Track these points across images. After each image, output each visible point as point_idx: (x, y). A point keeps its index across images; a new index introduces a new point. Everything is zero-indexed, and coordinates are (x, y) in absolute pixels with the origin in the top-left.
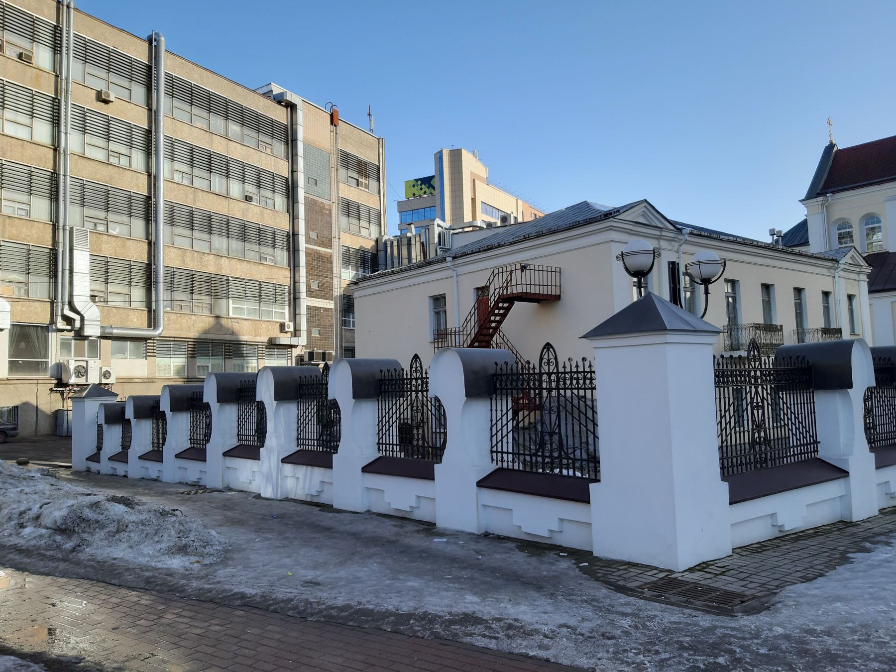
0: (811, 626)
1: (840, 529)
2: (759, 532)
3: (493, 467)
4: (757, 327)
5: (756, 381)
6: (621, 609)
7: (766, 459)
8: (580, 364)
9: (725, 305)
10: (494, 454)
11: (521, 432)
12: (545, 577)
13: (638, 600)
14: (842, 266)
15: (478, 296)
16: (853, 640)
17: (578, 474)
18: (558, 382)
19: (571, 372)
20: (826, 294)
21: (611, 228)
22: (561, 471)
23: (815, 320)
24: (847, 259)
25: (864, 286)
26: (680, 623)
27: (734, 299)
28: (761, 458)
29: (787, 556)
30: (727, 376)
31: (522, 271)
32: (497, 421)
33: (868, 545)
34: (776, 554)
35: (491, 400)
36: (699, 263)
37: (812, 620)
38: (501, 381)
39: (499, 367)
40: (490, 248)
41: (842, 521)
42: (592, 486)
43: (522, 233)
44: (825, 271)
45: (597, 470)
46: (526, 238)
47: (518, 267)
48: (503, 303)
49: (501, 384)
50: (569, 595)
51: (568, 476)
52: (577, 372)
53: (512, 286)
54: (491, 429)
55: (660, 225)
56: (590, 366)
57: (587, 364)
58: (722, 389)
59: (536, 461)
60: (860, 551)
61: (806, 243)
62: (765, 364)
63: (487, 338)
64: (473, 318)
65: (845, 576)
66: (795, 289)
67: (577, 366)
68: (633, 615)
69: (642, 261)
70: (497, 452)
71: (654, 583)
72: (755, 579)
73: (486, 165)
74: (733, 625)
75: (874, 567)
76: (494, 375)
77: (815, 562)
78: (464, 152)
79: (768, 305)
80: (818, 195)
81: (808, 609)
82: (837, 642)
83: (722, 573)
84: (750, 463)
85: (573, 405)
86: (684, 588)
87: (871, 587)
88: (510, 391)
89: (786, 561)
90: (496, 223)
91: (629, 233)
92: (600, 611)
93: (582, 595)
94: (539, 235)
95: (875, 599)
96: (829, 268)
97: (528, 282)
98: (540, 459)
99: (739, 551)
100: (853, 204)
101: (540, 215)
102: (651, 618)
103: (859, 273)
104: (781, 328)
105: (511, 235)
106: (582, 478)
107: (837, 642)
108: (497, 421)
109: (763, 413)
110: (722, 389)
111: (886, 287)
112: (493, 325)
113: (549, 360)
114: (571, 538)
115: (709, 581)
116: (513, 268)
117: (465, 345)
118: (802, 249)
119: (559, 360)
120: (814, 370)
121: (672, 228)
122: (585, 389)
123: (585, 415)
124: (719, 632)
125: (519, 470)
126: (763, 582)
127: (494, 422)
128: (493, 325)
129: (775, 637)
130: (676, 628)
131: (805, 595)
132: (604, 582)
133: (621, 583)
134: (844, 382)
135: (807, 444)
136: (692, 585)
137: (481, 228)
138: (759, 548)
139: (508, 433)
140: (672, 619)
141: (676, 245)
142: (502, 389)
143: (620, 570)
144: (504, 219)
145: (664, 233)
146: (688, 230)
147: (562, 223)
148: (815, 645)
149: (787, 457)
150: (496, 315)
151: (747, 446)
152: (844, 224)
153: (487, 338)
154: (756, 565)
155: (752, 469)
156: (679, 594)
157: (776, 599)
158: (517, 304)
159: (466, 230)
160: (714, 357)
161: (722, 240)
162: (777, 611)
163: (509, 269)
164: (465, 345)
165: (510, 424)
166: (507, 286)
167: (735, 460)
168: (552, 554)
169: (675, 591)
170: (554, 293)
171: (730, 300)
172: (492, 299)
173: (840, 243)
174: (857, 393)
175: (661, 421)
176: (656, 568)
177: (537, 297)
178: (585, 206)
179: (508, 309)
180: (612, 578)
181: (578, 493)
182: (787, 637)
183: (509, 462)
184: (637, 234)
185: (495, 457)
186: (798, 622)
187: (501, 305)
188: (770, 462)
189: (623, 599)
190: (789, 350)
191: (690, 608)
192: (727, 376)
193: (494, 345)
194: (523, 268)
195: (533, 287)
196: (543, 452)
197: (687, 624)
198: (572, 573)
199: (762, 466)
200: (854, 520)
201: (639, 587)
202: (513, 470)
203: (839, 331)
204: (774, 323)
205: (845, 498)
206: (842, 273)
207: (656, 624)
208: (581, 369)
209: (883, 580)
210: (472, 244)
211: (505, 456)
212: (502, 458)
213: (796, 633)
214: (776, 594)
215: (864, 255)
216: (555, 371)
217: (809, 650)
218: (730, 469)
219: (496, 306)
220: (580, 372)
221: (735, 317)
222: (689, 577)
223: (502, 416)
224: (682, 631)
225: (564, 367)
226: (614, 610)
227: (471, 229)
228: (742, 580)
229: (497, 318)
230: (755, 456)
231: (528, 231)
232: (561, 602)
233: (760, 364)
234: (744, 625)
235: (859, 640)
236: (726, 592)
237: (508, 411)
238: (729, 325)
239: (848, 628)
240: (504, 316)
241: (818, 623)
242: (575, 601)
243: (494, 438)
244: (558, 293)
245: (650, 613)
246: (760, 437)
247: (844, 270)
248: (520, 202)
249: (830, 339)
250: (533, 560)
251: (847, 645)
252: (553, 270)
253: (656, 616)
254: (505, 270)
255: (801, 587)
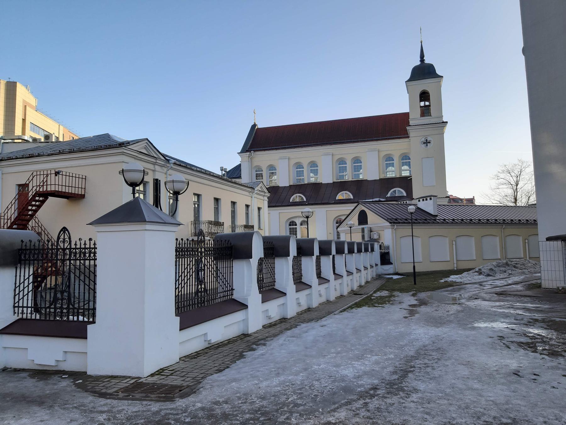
0: (218, 399)
1: (241, 339)
2: (196, 346)
3: (16, 318)
4: (210, 223)
5: (201, 254)
6: (100, 409)
7: (204, 301)
8: (88, 242)
9: (193, 209)
10: (16, 309)
11: (48, 291)
12: (48, 394)
13: (113, 401)
14: (256, 192)
15: (19, 190)
16: (239, 403)
17: (81, 318)
18: (70, 255)
19: (80, 248)
20: (247, 206)
21: (123, 154)
22: (68, 318)
23: (241, 220)
24: (258, 188)
25: (266, 203)
26: (139, 411)
27: (198, 205)
28: (201, 300)
29: (211, 358)
30: (184, 251)
31: (56, 175)
32: (20, 284)
33: (254, 346)
34: (205, 358)
35: (16, 268)
36: (173, 181)
37: (219, 396)
38: (25, 254)
39: (24, 244)
40: (31, 156)
41: (243, 334)
42: (89, 327)
43: (57, 149)
44: (247, 193)
45: (94, 315)
46: (60, 153)
47: (53, 172)
48: (40, 197)
49: (25, 257)
50: (64, 406)
51: (73, 321)
52: (85, 248)
53: (47, 185)
54: (15, 290)
55: (155, 156)
56: (95, 244)
57: (92, 242)
58: (186, 259)
59: (50, 312)
60: (250, 350)
61: (240, 177)
62: (207, 244)
63: (24, 223)
64: (13, 207)
65: (240, 366)
66: (232, 202)
67: (85, 244)
68: (108, 411)
69: (137, 177)
70: (18, 307)
71: (127, 387)
72: (191, 375)
73: (36, 97)
74: (172, 407)
75: (255, 359)
76: (19, 250)
77: (226, 360)
78: (19, 85)
79: (217, 210)
80: (247, 151)
81: (218, 389)
82: (230, 406)
83: (171, 374)
84: (195, 304)
85: (90, 271)
86: (145, 388)
87: (252, 371)
88: (32, 262)
89: (210, 361)
90: (40, 139)
91: (135, 158)
92: (85, 413)
93: (74, 404)
94: (71, 152)
95: (252, 377)
96: (250, 192)
97: (64, 184)
98: (52, 310)
99: (184, 358)
100: (265, 158)
101: (76, 138)
102: (120, 412)
103: (264, 196)
104: (223, 224)
105: (50, 148)
106: (83, 321)
107: (230, 406)
108: (20, 284)
109: (204, 273)
110: (186, 259)
111: (277, 205)
112: (30, 213)
113: (64, 239)
114: (72, 365)
115: (161, 381)
116: (49, 172)
117: (5, 227)
118: (237, 180)
119: (72, 239)
120: (232, 249)
121: (163, 159)
122: (90, 260)
123: (90, 276)
124: (163, 413)
125: (35, 319)
126: (194, 376)
127: (18, 285)
128: (30, 213)
129: (196, 410)
130: (136, 416)
131: (217, 381)
132: (92, 392)
133: (104, 391)
134: (249, 256)
135: (228, 291)
136: (151, 385)
137: (27, 141)
138: (196, 355)
139: (28, 292)
140: (134, 410)
141: (165, 169)
142: (25, 260)
143: (104, 382)
144: (47, 137)
145: (158, 161)
146: (173, 161)
147: (89, 146)
148: (218, 411)
149: (216, 299)
150: (33, 206)
151: (194, 295)
152: (259, 169)
153: (24, 223)
154: (193, 366)
155: (193, 308)
156: (141, 392)
157: (201, 385)
158: (50, 199)
159: (16, 141)
160: (177, 239)
161: (193, 170)
162: (200, 393)
163: (45, 173)
164: (5, 227)
165: (31, 286)
166: (43, 186)
167: (186, 302)
168: (56, 377)
169: (139, 391)
170: (80, 193)
171: (196, 206)
172: (30, 194)
173: (257, 179)
174: (290, 258)
175: (135, 280)
176: (129, 377)
177: (66, 195)
178: (107, 136)
179: (43, 202)
180: (97, 389)
181: (80, 332)
182: (203, 409)
183: (28, 314)
184: (141, 160)
185: (16, 311)
186: (210, 398)
187: (37, 198)
188: (206, 303)
189: (103, 401)
190: (228, 236)
191: (147, 400)
192: (184, 251)
193: (30, 228)
194: (57, 173)
195: (64, 187)
196: (55, 306)
197: (144, 411)
198: (69, 389)
199: (201, 305)
200: (250, 333)
201: (116, 392)
202: (31, 319)
203: (252, 227)
204: (220, 221)
205: (245, 321)
206: (256, 195)
207: (123, 415)
208: (87, 246)
209: (259, 365)
210: (17, 152)
211: (25, 309)
212: (23, 311)
213: (208, 405)
214: (201, 382)
215: (267, 187)
216: (69, 247)
217: (214, 414)
218: (183, 309)
219: (33, 199)
220: (78, 249)
221: (199, 216)
222: (151, 380)
223: (24, 280)
224: (139, 416)
225: (76, 245)
226: (95, 410)
227: (20, 141)
228: (183, 377)
229: (34, 208)
230: (198, 300)
231: (63, 148)
232: (57, 411)
233: (205, 244)
234: (179, 406)
235: (242, 403)
236: (172, 386)
237: (29, 276)
238: (195, 220)
239: (237, 397)
240: (39, 207)
241: (222, 397)
242: (67, 409)
243: (17, 297)
244: (83, 193)
245: (120, 408)
246: (201, 288)
247: (257, 194)
248: (61, 127)
249: (247, 231)
250: (41, 384)
251: (235, 407)
252: (81, 176)
253: (123, 409)
254: (42, 173)
255: (215, 376)
